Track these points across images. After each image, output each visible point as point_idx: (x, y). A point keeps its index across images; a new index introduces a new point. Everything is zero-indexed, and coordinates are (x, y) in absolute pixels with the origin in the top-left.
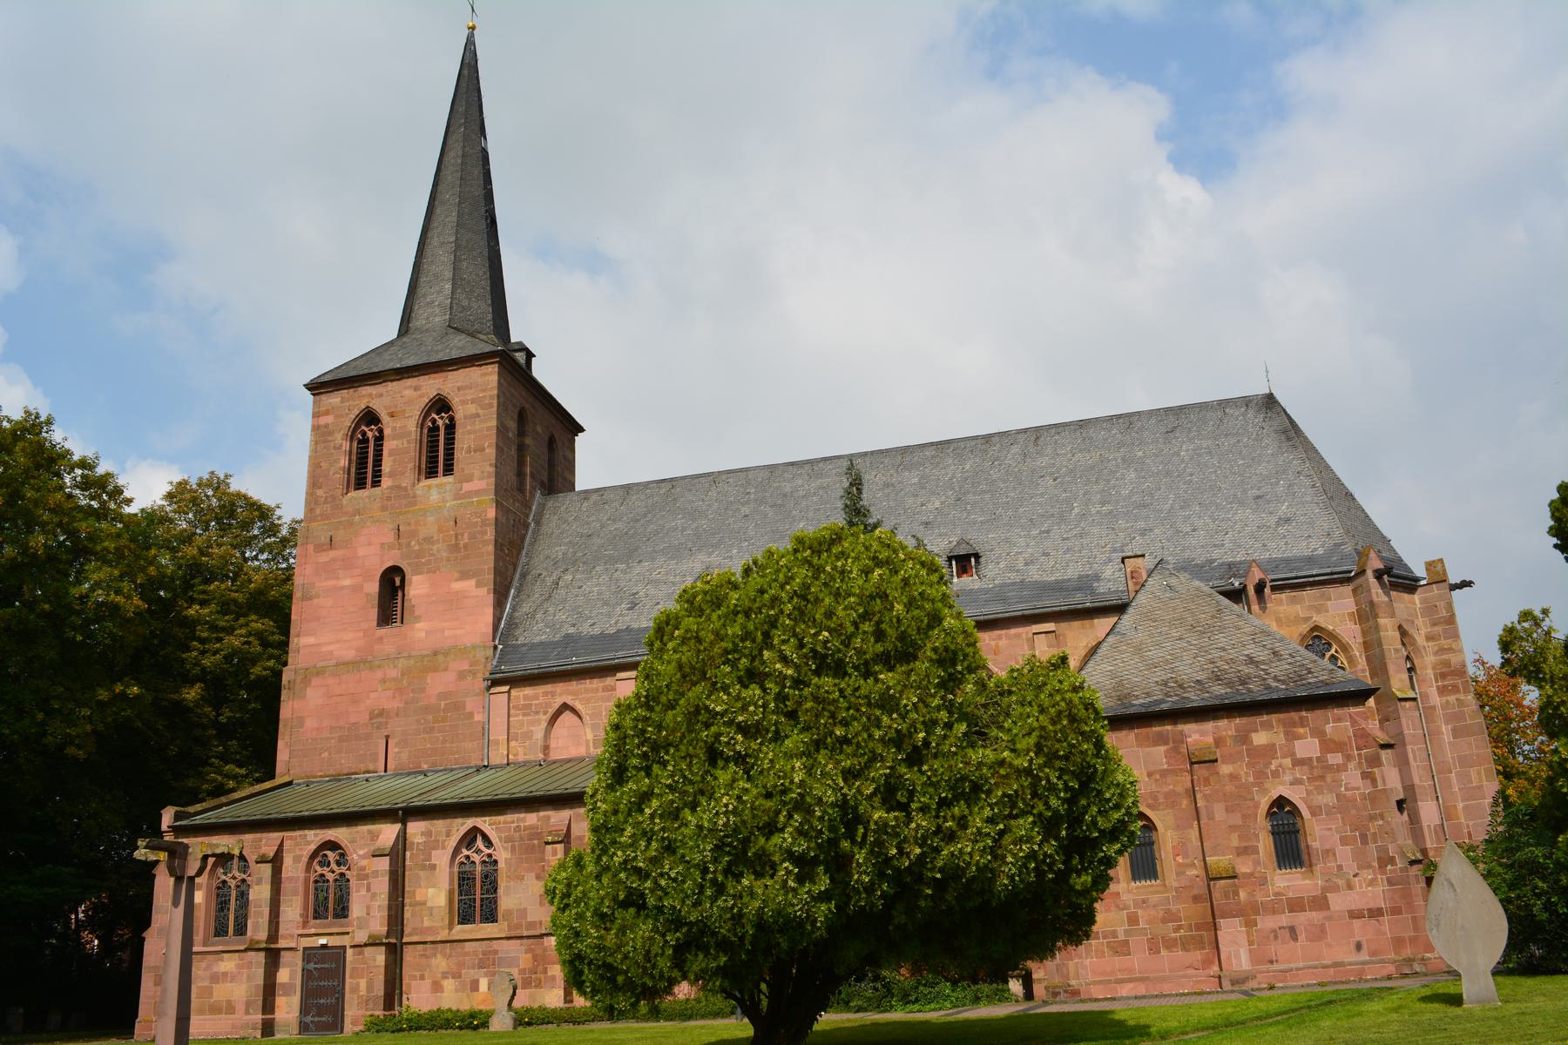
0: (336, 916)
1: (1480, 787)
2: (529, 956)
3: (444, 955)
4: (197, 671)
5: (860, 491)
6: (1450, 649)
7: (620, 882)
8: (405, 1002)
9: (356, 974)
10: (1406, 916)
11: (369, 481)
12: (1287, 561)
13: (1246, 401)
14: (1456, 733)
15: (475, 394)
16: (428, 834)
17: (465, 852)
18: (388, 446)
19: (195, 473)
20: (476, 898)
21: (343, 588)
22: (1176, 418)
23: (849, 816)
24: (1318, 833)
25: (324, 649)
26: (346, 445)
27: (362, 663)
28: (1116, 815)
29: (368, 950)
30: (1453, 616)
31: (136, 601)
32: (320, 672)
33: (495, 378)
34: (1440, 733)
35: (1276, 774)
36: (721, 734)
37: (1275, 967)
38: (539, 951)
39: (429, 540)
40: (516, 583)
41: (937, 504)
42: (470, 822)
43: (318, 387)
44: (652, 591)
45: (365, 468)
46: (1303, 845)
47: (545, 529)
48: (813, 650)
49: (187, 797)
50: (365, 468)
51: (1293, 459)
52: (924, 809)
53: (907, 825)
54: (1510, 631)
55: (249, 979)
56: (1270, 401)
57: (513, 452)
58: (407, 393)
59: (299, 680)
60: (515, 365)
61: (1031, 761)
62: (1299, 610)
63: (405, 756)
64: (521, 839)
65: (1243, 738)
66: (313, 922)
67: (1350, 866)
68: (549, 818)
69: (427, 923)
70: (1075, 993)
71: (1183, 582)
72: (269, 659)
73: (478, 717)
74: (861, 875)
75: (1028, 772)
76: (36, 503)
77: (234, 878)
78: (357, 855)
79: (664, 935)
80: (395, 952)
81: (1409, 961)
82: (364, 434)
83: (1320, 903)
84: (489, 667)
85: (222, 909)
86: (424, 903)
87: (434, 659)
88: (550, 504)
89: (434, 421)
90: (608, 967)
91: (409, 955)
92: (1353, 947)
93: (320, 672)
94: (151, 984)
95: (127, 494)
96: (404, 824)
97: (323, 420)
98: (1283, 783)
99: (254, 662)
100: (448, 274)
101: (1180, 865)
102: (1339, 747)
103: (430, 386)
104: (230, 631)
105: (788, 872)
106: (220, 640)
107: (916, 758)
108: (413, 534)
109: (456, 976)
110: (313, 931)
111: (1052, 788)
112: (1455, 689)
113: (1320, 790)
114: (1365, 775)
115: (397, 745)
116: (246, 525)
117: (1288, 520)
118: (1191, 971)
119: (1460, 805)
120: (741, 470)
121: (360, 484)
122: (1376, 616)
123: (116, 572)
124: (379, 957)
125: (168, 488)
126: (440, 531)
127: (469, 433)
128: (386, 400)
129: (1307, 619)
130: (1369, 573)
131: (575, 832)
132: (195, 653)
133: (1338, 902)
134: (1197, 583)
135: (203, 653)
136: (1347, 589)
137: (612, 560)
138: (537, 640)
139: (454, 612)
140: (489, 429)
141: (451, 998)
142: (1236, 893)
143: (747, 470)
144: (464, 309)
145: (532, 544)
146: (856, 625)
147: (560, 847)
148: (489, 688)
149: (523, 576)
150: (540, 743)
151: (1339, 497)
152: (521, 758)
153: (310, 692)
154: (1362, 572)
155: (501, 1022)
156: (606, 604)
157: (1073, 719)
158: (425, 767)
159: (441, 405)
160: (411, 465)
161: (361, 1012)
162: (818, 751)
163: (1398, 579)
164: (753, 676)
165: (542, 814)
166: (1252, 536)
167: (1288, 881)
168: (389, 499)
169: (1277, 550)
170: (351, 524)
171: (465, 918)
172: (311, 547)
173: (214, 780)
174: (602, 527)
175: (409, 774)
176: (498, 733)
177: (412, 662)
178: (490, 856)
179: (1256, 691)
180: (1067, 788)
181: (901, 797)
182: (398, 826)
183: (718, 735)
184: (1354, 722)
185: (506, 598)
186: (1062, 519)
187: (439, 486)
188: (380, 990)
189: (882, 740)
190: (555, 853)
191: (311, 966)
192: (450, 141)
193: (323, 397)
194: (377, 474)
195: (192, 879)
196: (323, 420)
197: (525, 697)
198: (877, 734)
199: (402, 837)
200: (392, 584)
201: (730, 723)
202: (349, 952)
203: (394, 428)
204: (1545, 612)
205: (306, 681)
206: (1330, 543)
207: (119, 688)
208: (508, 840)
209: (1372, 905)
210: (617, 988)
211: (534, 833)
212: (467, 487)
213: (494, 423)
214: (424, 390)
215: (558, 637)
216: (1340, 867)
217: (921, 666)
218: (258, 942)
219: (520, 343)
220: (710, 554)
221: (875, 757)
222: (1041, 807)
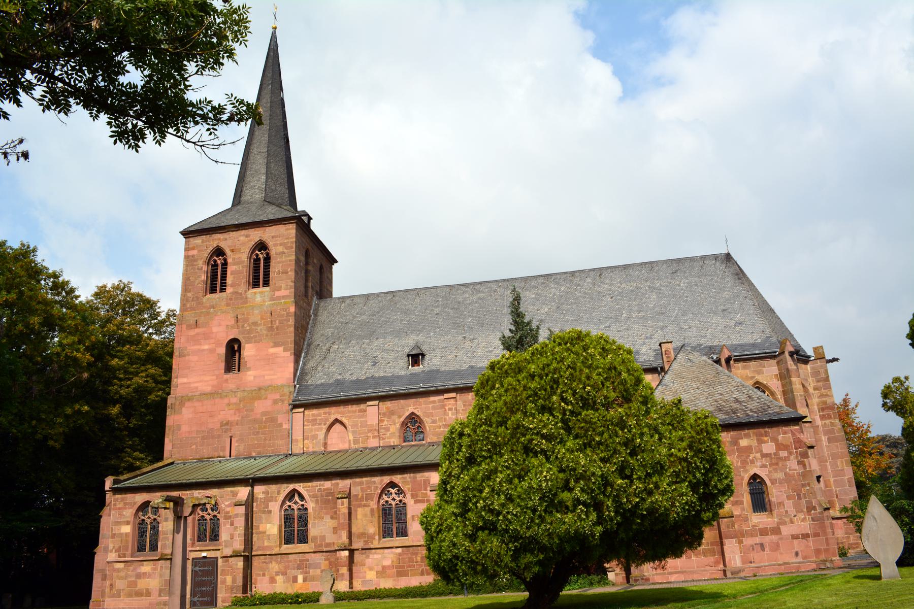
0: (211, 540)
1: (843, 470)
3: (277, 562)
4: (117, 397)
5: (519, 303)
6: (827, 395)
7: (481, 516)
8: (254, 589)
9: (224, 573)
10: (822, 538)
11: (218, 288)
12: (741, 346)
13: (716, 257)
14: (830, 440)
15: (282, 241)
16: (266, 493)
17: (288, 503)
18: (230, 269)
19: (110, 282)
20: (295, 529)
21: (204, 350)
22: (677, 265)
23: (606, 482)
24: (775, 493)
25: (192, 385)
26: (205, 268)
28: (726, 482)
29: (231, 560)
30: (828, 377)
31: (88, 356)
33: (294, 231)
34: (821, 440)
35: (752, 462)
36: (533, 440)
37: (753, 565)
38: (332, 560)
39: (255, 324)
40: (305, 350)
41: (546, 310)
42: (291, 486)
43: (187, 233)
44: (385, 356)
45: (216, 280)
46: (766, 500)
47: (319, 318)
48: (581, 396)
49: (116, 472)
50: (216, 280)
51: (741, 289)
52: (639, 478)
53: (631, 486)
54: (888, 387)
55: (161, 576)
57: (303, 272)
58: (242, 238)
59: (177, 403)
60: (302, 222)
61: (687, 454)
62: (748, 373)
63: (242, 448)
64: (322, 496)
65: (735, 442)
66: (197, 543)
67: (792, 511)
68: (338, 484)
69: (266, 544)
70: (647, 580)
71: (696, 357)
72: (159, 391)
73: (285, 426)
74: (610, 512)
75: (685, 459)
76: (31, 298)
77: (149, 518)
78: (224, 505)
79: (507, 544)
80: (248, 560)
81: (824, 562)
82: (215, 261)
83: (776, 531)
84: (292, 398)
85: (142, 536)
86: (264, 532)
87: (259, 392)
88: (322, 304)
89: (257, 255)
90: (472, 562)
91: (256, 562)
92: (794, 554)
93: (190, 399)
95: (77, 293)
96: (252, 487)
97: (191, 253)
98: (756, 467)
99: (150, 393)
100: (264, 170)
102: (786, 447)
103: (256, 235)
104: (136, 374)
105: (582, 511)
106: (130, 379)
107: (633, 454)
108: (246, 320)
109: (284, 574)
110: (198, 548)
111: (697, 468)
112: (829, 417)
113: (776, 470)
114: (799, 463)
115: (237, 441)
116: (141, 312)
117: (741, 323)
118: (709, 568)
119: (832, 480)
120: (433, 288)
121: (213, 290)
122: (790, 377)
123: (76, 339)
124: (240, 563)
125: (96, 290)
126: (262, 318)
127: (279, 262)
128: (229, 242)
129: (752, 378)
130: (787, 354)
131: (353, 492)
132: (116, 387)
133: (786, 530)
134: (704, 358)
135: (121, 386)
136: (774, 362)
137: (361, 337)
138: (319, 382)
139: (270, 366)
140: (290, 261)
141: (281, 586)
142: (733, 526)
143: (437, 287)
144: (273, 191)
145: (313, 327)
146: (603, 384)
147: (346, 501)
148: (292, 410)
149: (309, 345)
150: (322, 441)
151: (767, 311)
152: (311, 450)
153: (184, 410)
154: (782, 353)
155: (327, 599)
156: (358, 362)
157: (708, 433)
158: (254, 454)
159: (262, 246)
160: (244, 280)
161: (228, 595)
162: (585, 448)
163: (800, 357)
164: (546, 409)
165: (334, 482)
166: (722, 331)
167: (759, 519)
168: (231, 299)
169: (735, 340)
170: (208, 313)
171: (288, 540)
172: (184, 326)
173: (128, 461)
174: (354, 318)
175: (245, 458)
176: (298, 435)
177: (245, 394)
178: (303, 505)
179: (741, 417)
180: (704, 468)
181: (627, 472)
182: (249, 488)
183: (531, 440)
184: (793, 434)
185: (300, 357)
186: (617, 320)
187: (261, 293)
188: (240, 582)
189: (619, 443)
190: (343, 504)
191: (197, 569)
192: (263, 93)
193: (191, 239)
195: (186, 517)
196: (191, 253)
197: (313, 415)
198: (617, 440)
199: (252, 494)
200: (233, 349)
201: (537, 434)
202: (220, 560)
203: (234, 259)
204: (907, 378)
205: (182, 404)
206: (764, 336)
207: (77, 407)
208: (314, 496)
209: (803, 532)
210: (476, 573)
211: (329, 493)
212: (277, 294)
213: (294, 257)
214: (251, 237)
215: (331, 381)
216: (787, 512)
217: (635, 405)
219: (304, 211)
220: (418, 335)
221: (615, 452)
222: (691, 477)
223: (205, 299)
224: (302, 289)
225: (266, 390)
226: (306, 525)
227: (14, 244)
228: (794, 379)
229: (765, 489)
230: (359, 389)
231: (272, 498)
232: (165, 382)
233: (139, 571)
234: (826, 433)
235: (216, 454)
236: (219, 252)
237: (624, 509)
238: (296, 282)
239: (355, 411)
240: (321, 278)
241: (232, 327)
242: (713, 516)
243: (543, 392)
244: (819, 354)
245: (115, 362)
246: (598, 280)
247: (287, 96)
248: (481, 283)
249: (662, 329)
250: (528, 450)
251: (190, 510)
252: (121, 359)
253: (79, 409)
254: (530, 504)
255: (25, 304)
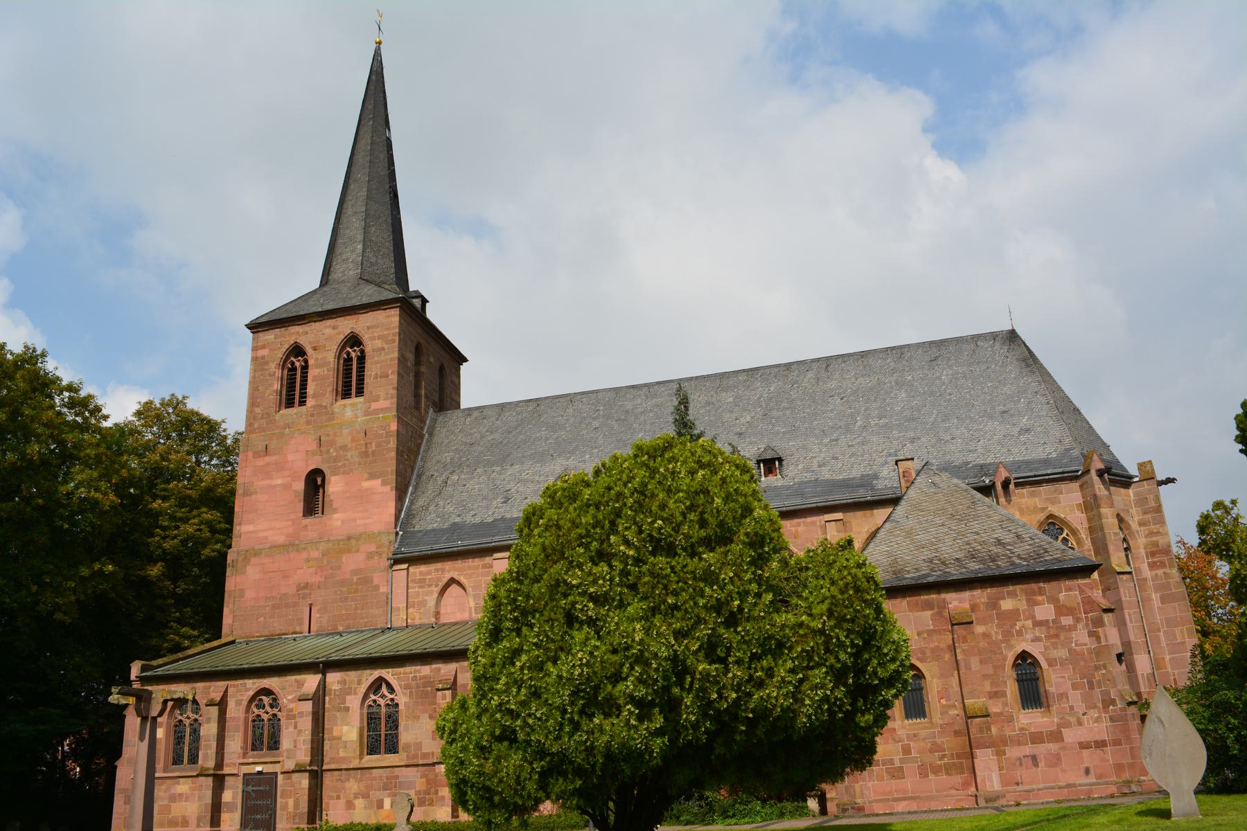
0: (270, 748)
1: (1183, 643)
2: (424, 780)
6: (1158, 533)
8: (324, 817)
12: (1027, 463)
13: (994, 336)
14: (1163, 599)
15: (381, 332)
16: (343, 682)
17: (373, 697)
18: (312, 373)
19: (157, 396)
20: (381, 734)
21: (275, 486)
22: (938, 349)
23: (679, 668)
24: (1054, 680)
25: (261, 535)
26: (278, 373)
27: (288, 546)
28: (892, 667)
29: (295, 776)
31: (112, 497)
32: (257, 553)
33: (397, 319)
34: (1152, 600)
35: (1020, 633)
36: (576, 603)
37: (1020, 788)
38: (431, 777)
39: (344, 448)
40: (413, 482)
41: (748, 418)
42: (377, 673)
43: (256, 327)
45: (293, 390)
46: (1042, 690)
47: (435, 439)
48: (650, 535)
49: (150, 653)
50: (293, 390)
52: (739, 662)
53: (725, 675)
54: (1206, 517)
55: (200, 798)
56: (1012, 336)
57: (412, 378)
58: (327, 331)
59: (241, 559)
60: (412, 310)
62: (1037, 502)
63: (324, 620)
65: (993, 604)
66: (251, 753)
67: (1080, 707)
68: (439, 670)
69: (342, 754)
71: (944, 480)
72: (217, 543)
73: (383, 589)
74: (689, 715)
75: (822, 632)
77: (188, 718)
78: (287, 699)
79: (531, 764)
80: (316, 777)
81: (1128, 783)
82: (293, 363)
83: (1056, 736)
84: (392, 549)
85: (179, 743)
86: (340, 738)
87: (349, 543)
88: (440, 419)
89: (348, 354)
90: (487, 789)
91: (328, 780)
92: (1082, 771)
93: (257, 553)
94: (121, 803)
95: (105, 412)
97: (260, 353)
98: (1025, 641)
99: (204, 545)
100: (360, 237)
101: (943, 706)
102: (1070, 611)
103: (346, 325)
104: (185, 520)
105: (631, 713)
106: (177, 528)
107: (732, 621)
110: (251, 760)
111: (841, 645)
112: (1163, 565)
113: (1055, 646)
114: (1091, 634)
115: (319, 611)
117: (1028, 430)
118: (953, 792)
119: (1168, 658)
120: (592, 392)
121: (290, 403)
122: (1099, 507)
123: (95, 474)
124: (304, 781)
125: (137, 407)
126: (353, 440)
127: (376, 362)
129: (1043, 509)
130: (1093, 472)
131: (460, 681)
133: (1070, 736)
134: (955, 481)
135: (164, 538)
136: (1075, 485)
137: (490, 464)
138: (430, 527)
139: (364, 506)
140: (392, 359)
141: (361, 814)
142: (989, 729)
143: (597, 392)
144: (372, 265)
145: (426, 451)
146: (684, 514)
147: (448, 693)
148: (392, 566)
149: (419, 476)
150: (433, 610)
151: (1068, 412)
152: (417, 622)
153: (250, 570)
154: (1088, 471)
156: (485, 498)
158: (341, 629)
159: (354, 340)
160: (330, 389)
162: (654, 615)
163: (1116, 477)
164: (602, 556)
165: (434, 666)
166: (999, 443)
167: (1030, 719)
168: (312, 415)
169: (1019, 454)
170: (282, 435)
171: (373, 750)
172: (250, 454)
173: (173, 640)
174: (482, 437)
175: (328, 635)
176: (399, 602)
177: (330, 545)
178: (392, 700)
179: (1003, 567)
180: (853, 645)
181: (721, 652)
182: (319, 676)
183: (574, 603)
184: (1082, 591)
185: (406, 493)
186: (848, 430)
188: (304, 807)
189: (705, 606)
190: (444, 697)
191: (250, 788)
193: (260, 334)
194: (303, 396)
195: (154, 719)
196: (260, 353)
197: (421, 573)
198: (701, 602)
199: (323, 685)
200: (315, 483)
201: (584, 593)
202: (280, 777)
203: (317, 359)
204: (1234, 502)
205: (246, 560)
206: (1061, 448)
207: (97, 566)
208: (407, 687)
209: (1098, 738)
210: (494, 806)
211: (427, 682)
212: (374, 406)
213: (396, 355)
214: (340, 329)
216: (1072, 708)
218: (208, 769)
220: (568, 459)
221: (699, 621)
222: (832, 660)
223: (278, 417)
224: (411, 398)
225: (358, 539)
226: (397, 728)
227: (15, 346)
228: (1105, 511)
229: (1039, 673)
230: (483, 536)
231: (349, 690)
232: (224, 531)
233: (173, 791)
234: (1157, 589)
235: (291, 629)
236: (297, 350)
237: (718, 711)
238: (399, 388)
239: (478, 567)
240: (440, 384)
241: (314, 453)
242: (876, 721)
243: (598, 530)
244: (1147, 472)
245: (156, 504)
246: (823, 374)
247: (396, 135)
248: (659, 383)
249: (912, 442)
250: (571, 620)
251: (159, 707)
252: (164, 499)
253: (101, 570)
254: (558, 701)
255: (17, 428)
